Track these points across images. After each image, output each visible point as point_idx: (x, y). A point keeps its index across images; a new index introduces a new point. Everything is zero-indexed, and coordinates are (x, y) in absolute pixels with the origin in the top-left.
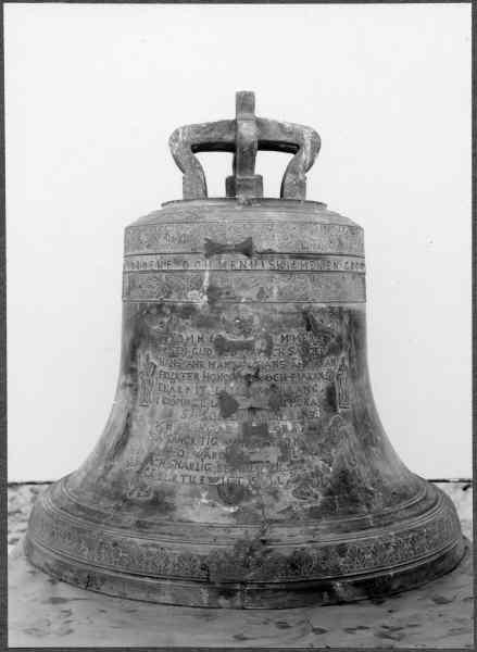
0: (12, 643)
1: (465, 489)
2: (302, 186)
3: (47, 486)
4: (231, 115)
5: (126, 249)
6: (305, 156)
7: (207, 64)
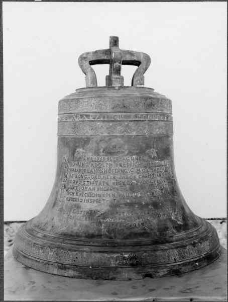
0: (5, 299)
1: (221, 223)
2: (142, 79)
3: (20, 225)
4: (107, 47)
5: (59, 111)
6: (143, 66)
7: (97, 26)
